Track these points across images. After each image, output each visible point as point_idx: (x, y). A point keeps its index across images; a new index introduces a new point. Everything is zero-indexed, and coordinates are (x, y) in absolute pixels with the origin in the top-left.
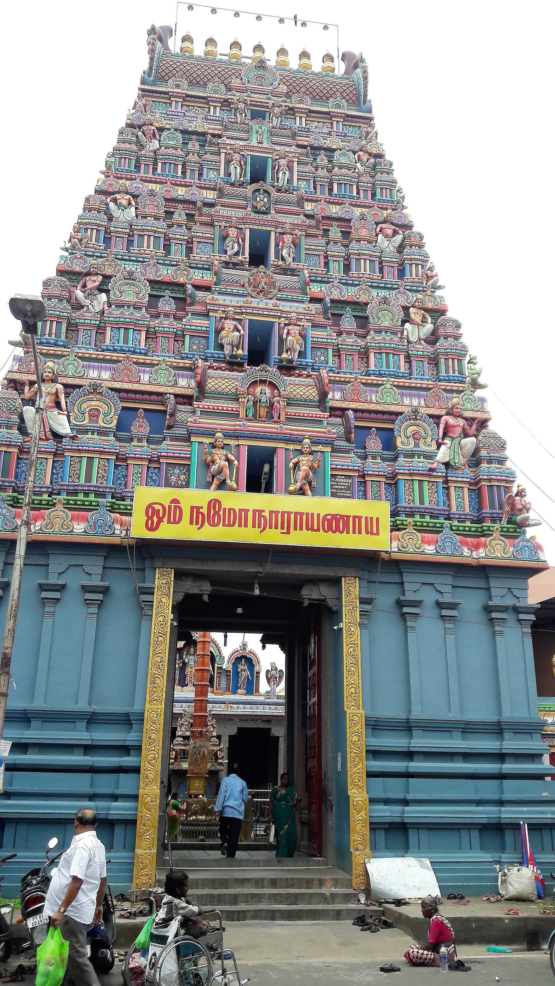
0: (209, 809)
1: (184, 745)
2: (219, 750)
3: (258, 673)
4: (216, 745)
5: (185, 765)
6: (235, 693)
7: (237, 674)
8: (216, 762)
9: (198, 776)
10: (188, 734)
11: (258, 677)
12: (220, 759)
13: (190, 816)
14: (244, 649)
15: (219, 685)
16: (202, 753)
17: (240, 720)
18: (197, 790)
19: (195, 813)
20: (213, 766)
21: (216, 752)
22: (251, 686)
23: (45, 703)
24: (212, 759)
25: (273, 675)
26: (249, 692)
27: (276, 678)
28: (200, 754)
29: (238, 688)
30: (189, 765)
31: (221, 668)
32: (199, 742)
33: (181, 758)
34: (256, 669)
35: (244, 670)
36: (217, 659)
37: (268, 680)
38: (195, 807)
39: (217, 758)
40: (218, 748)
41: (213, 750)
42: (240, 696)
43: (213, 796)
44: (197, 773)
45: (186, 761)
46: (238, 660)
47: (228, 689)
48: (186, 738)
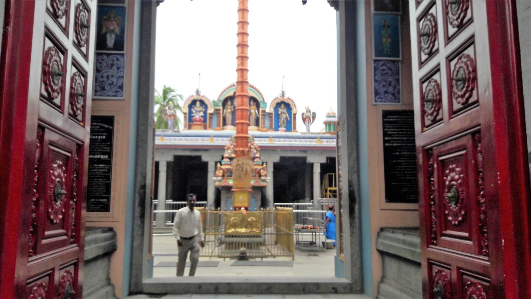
0: (248, 222)
1: (230, 165)
2: (262, 169)
3: (295, 115)
4: (259, 165)
5: (231, 182)
6: (277, 130)
7: (278, 116)
8: (260, 179)
9: (242, 190)
10: (233, 155)
11: (295, 118)
12: (263, 176)
13: (229, 228)
14: (283, 95)
15: (264, 124)
16: (244, 170)
17: (282, 150)
18: (241, 203)
19: (235, 226)
20: (257, 182)
21: (259, 171)
22: (290, 125)
23: (327, 237)
24: (256, 176)
25: (307, 116)
26: (289, 129)
27: (310, 118)
28: (243, 170)
29: (279, 126)
30: (234, 181)
31: (264, 111)
32: (241, 160)
33: (228, 176)
34: (293, 111)
35: (284, 113)
36: (261, 105)
37: (304, 120)
38: (235, 219)
39: (260, 176)
40: (261, 167)
41: (256, 169)
42: (282, 132)
43: (259, 208)
44: (240, 188)
45: (231, 179)
46: (279, 105)
47: (271, 128)
48: (231, 159)
